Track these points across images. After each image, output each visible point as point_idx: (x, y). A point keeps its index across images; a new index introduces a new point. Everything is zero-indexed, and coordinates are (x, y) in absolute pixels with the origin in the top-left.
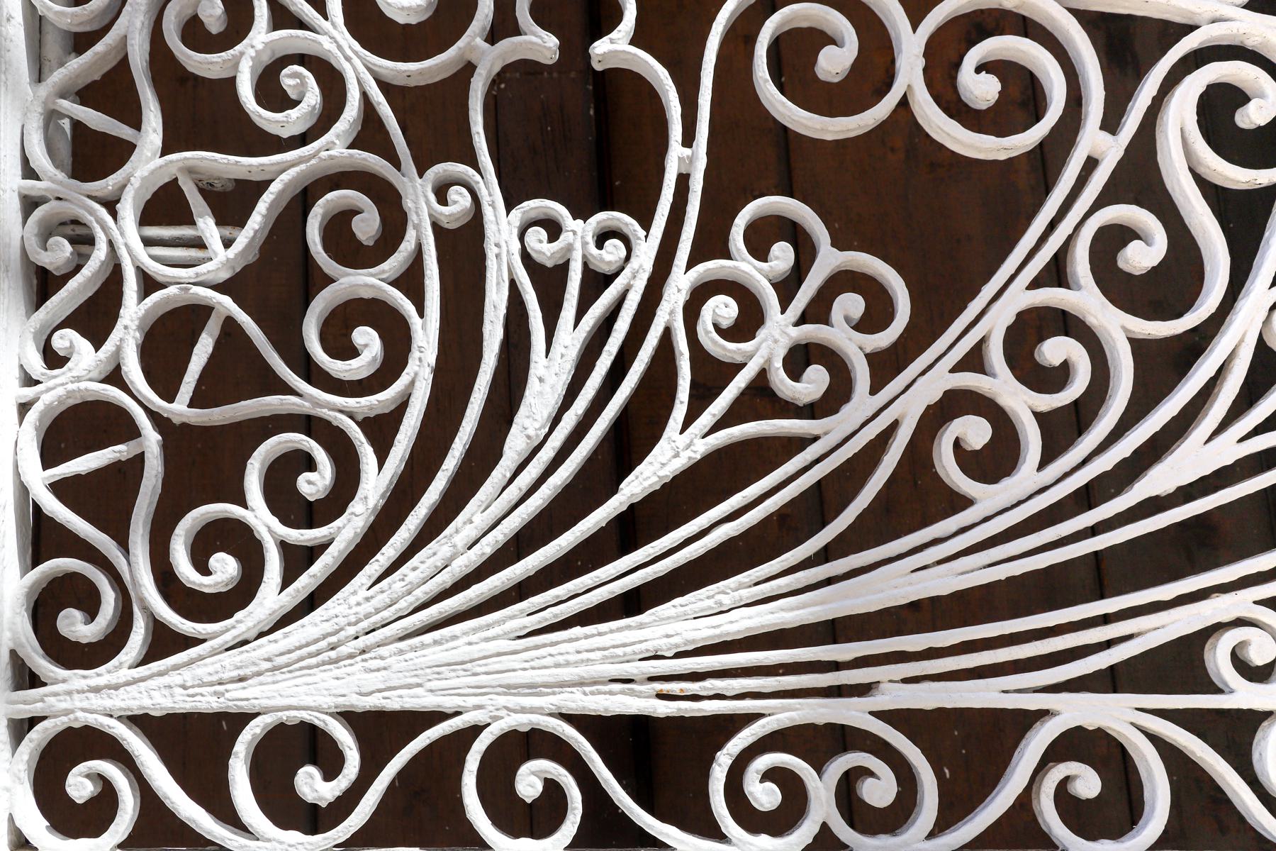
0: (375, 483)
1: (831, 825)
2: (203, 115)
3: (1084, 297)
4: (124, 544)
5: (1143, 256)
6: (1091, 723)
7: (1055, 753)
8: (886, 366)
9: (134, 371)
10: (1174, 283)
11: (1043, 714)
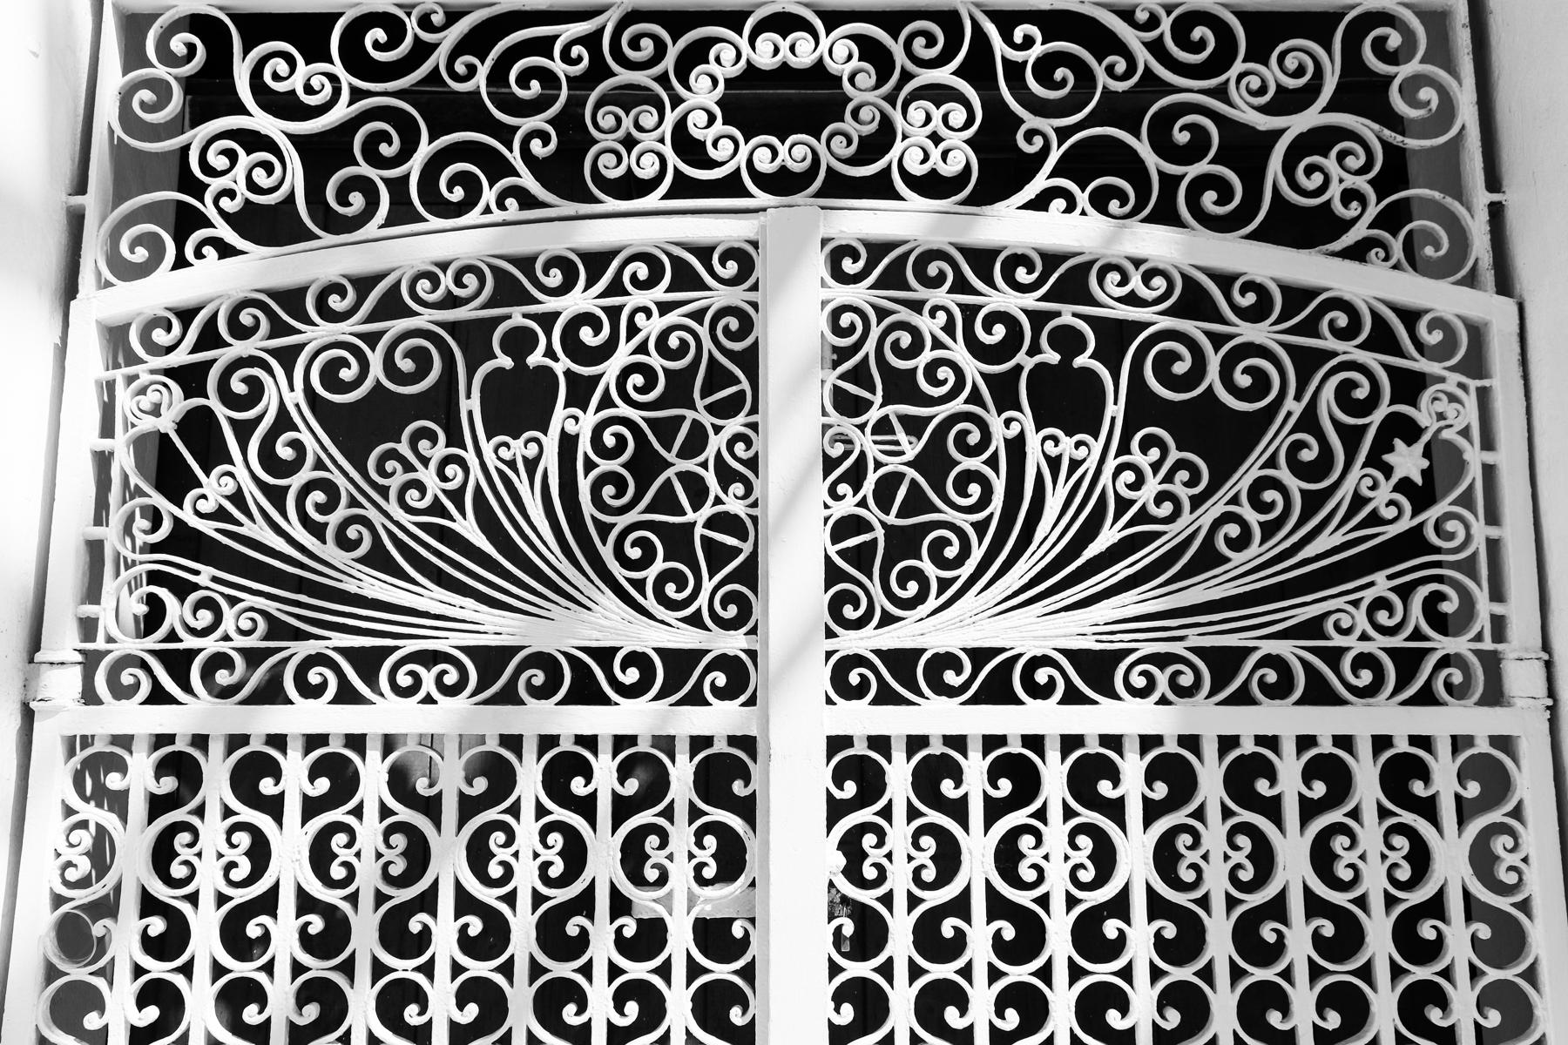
0: (977, 553)
1: (948, 733)
2: (901, 387)
3: (1284, 474)
4: (871, 579)
5: (1307, 455)
6: (1274, 652)
7: (1260, 664)
8: (1196, 502)
9: (871, 502)
10: (1324, 462)
11: (1255, 649)
